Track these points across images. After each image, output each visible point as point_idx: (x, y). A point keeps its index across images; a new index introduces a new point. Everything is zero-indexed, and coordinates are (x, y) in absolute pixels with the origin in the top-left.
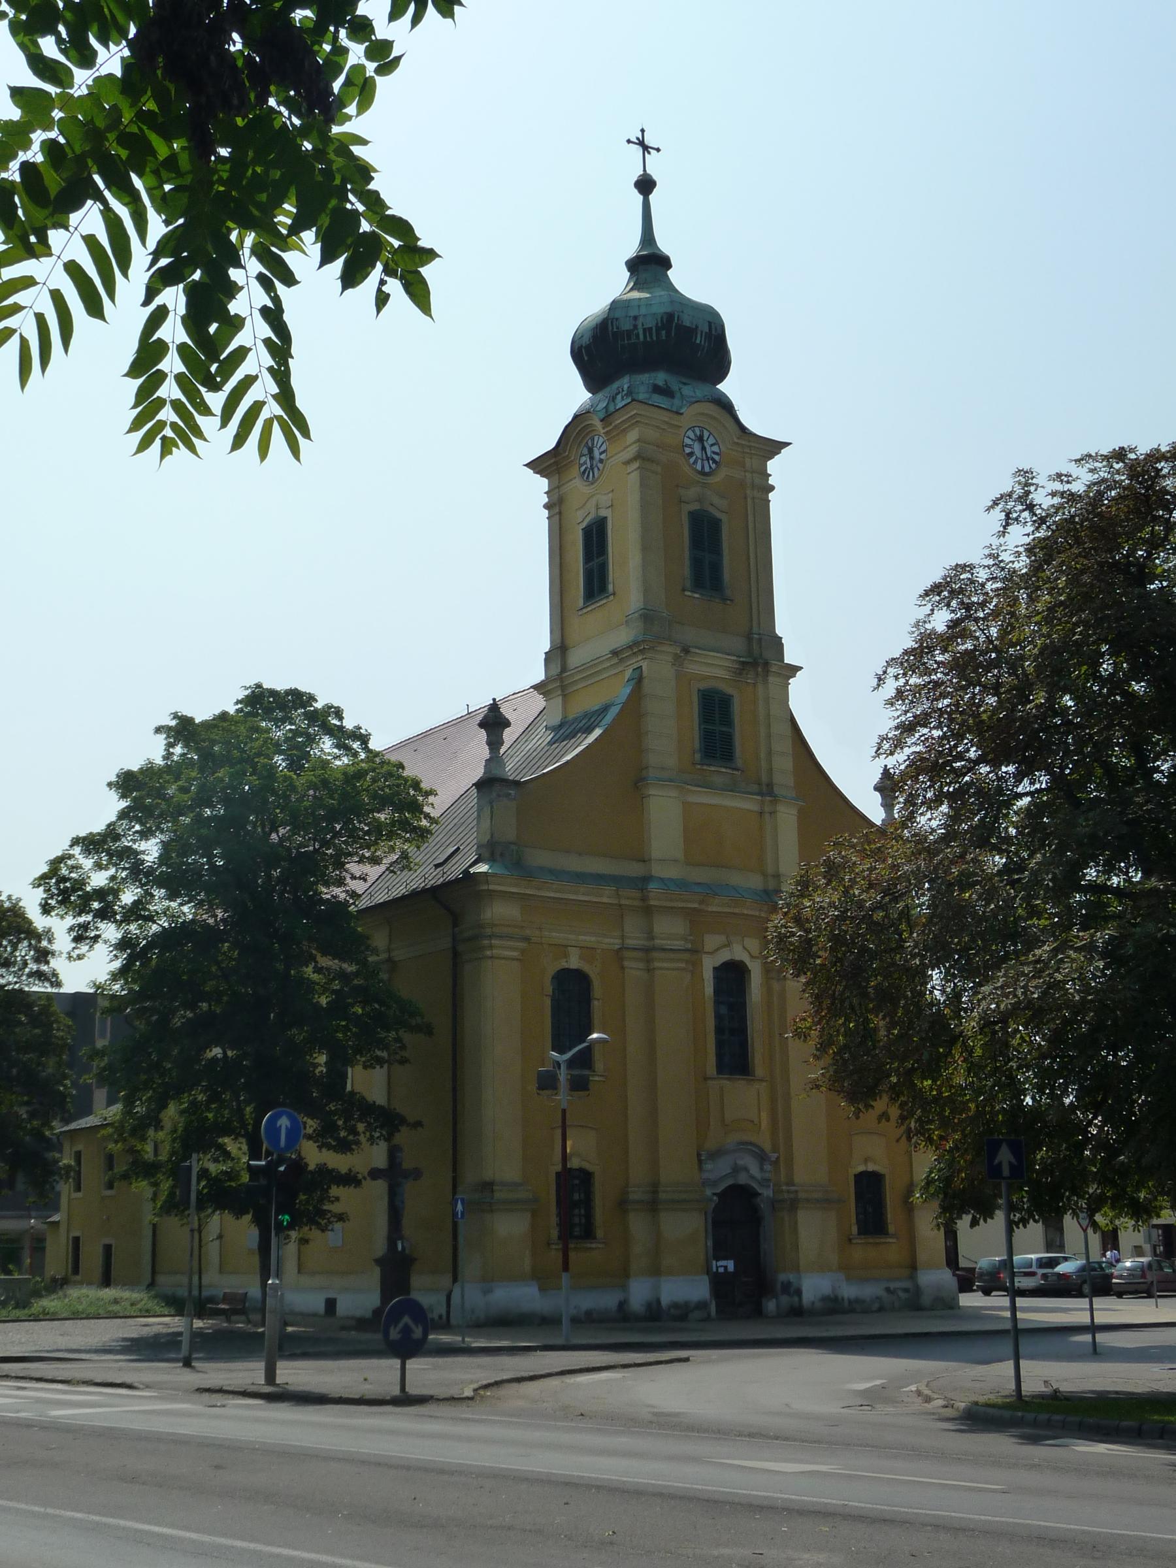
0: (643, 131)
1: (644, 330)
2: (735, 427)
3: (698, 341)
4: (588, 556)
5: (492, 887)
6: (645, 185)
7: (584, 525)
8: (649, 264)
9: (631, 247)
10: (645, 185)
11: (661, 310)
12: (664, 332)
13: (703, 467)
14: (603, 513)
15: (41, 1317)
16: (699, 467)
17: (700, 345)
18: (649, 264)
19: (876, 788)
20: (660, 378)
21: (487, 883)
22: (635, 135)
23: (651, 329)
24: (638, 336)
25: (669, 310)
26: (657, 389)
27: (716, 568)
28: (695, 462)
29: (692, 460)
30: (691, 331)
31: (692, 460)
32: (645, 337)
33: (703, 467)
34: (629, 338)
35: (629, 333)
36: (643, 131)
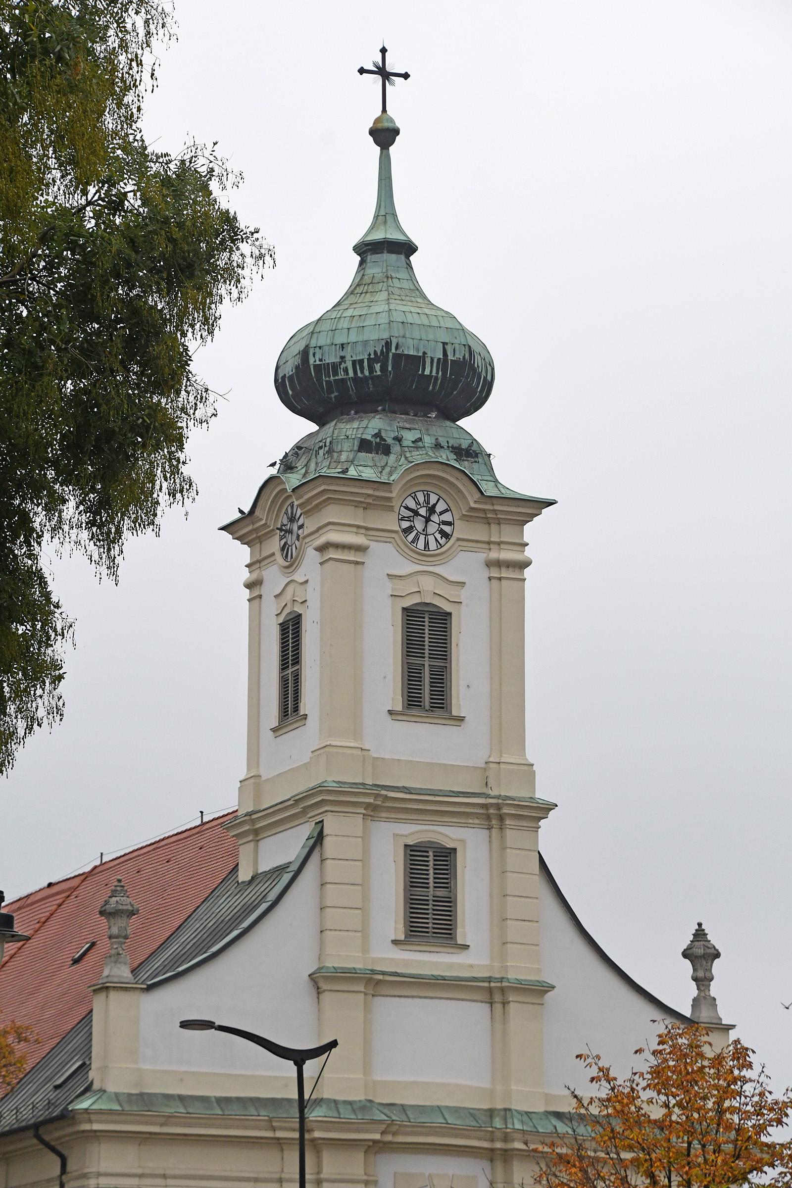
0: (384, 51)
1: (354, 362)
2: (477, 495)
3: (427, 372)
4: (284, 666)
5: (96, 1127)
6: (384, 135)
7: (281, 619)
8: (386, 250)
9: (359, 224)
10: (384, 135)
11: (373, 335)
12: (378, 367)
13: (427, 544)
14: (298, 609)
15: (148, 1136)
16: (421, 544)
17: (430, 376)
18: (386, 250)
19: (685, 955)
20: (374, 425)
21: (90, 1121)
22: (371, 59)
23: (361, 362)
24: (346, 370)
25: (385, 336)
26: (364, 446)
27: (411, 645)
28: (416, 539)
29: (411, 537)
30: (418, 361)
31: (411, 537)
32: (355, 372)
33: (427, 544)
34: (336, 373)
35: (335, 367)
36: (384, 51)
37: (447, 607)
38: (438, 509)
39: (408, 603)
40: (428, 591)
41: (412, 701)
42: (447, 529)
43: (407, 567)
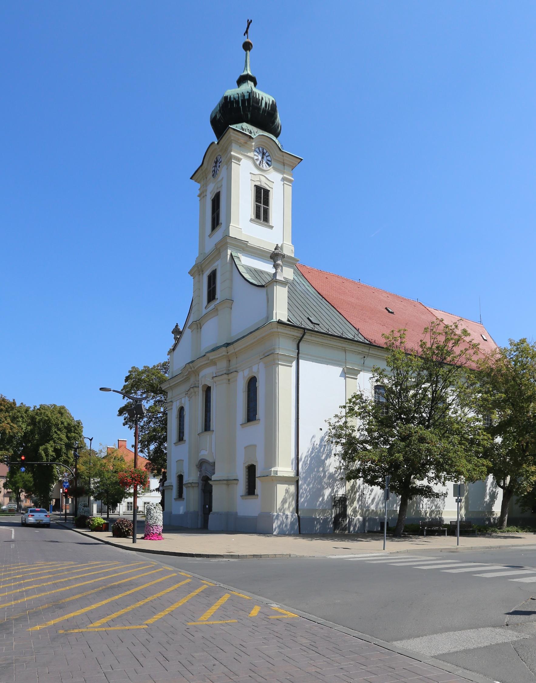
27: (258, 198)
30: (216, 116)
37: (269, 189)
38: (267, 154)
39: (258, 184)
40: (264, 184)
41: (258, 216)
42: (269, 162)
43: (257, 172)
